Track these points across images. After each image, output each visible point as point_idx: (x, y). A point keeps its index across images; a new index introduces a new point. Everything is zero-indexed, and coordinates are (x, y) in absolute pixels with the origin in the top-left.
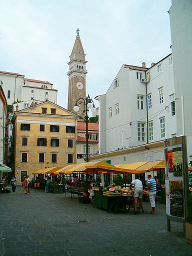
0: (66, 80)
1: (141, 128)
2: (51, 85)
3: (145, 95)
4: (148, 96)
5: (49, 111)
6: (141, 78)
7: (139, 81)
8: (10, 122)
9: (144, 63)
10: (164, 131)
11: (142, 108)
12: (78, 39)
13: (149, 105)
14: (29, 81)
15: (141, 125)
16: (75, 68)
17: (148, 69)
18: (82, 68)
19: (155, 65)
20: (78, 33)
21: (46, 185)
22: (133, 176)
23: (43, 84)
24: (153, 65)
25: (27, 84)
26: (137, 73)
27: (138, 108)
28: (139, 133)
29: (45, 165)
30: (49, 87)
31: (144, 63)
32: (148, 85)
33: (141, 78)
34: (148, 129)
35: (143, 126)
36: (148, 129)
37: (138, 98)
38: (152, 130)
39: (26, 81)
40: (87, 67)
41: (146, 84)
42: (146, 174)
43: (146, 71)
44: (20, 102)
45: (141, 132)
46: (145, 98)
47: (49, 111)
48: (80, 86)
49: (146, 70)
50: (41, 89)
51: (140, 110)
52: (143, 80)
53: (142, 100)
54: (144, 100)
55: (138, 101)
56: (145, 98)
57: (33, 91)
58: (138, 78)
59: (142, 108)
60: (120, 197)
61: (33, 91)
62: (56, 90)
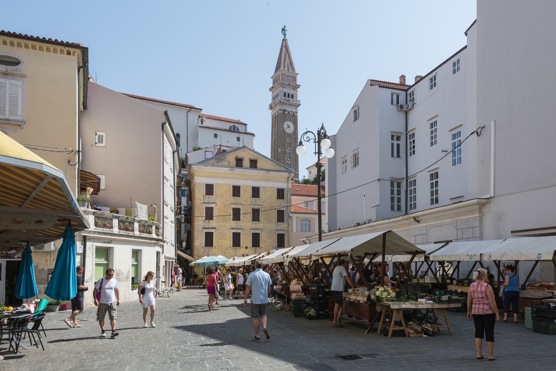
0: (268, 116)
1: (395, 189)
2: (243, 126)
3: (403, 130)
4: (410, 136)
5: (246, 163)
6: (398, 103)
7: (394, 108)
8: (231, 293)
9: (403, 78)
10: (432, 192)
11: (398, 156)
12: (285, 46)
13: (411, 150)
14: (209, 118)
15: (395, 183)
16: (281, 96)
17: (411, 87)
18: (292, 97)
19: (422, 78)
20: (285, 35)
21: (230, 279)
22: (446, 262)
23: (232, 124)
24: (418, 79)
25: (207, 123)
26: (392, 95)
27: (393, 156)
28: (392, 199)
29: (242, 250)
30: (241, 128)
31: (403, 78)
32: (411, 115)
33: (398, 103)
34: (407, 191)
35: (399, 185)
36: (407, 191)
37: (392, 139)
38: (415, 192)
39: (204, 119)
40: (301, 95)
41: (406, 112)
42: (446, 264)
43: (406, 91)
44: (199, 149)
45: (396, 196)
46: (403, 138)
47: (246, 163)
48: (288, 127)
49: (406, 88)
50: (230, 130)
51: (396, 160)
52: (402, 107)
53: (398, 142)
54: (402, 142)
55: (392, 144)
56: (403, 138)
57: (216, 136)
58: (392, 103)
59: (398, 156)
60: (55, 240)
61: (216, 136)
62: (253, 135)
